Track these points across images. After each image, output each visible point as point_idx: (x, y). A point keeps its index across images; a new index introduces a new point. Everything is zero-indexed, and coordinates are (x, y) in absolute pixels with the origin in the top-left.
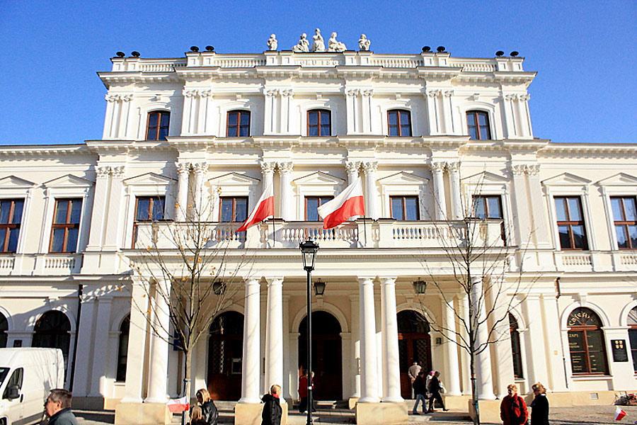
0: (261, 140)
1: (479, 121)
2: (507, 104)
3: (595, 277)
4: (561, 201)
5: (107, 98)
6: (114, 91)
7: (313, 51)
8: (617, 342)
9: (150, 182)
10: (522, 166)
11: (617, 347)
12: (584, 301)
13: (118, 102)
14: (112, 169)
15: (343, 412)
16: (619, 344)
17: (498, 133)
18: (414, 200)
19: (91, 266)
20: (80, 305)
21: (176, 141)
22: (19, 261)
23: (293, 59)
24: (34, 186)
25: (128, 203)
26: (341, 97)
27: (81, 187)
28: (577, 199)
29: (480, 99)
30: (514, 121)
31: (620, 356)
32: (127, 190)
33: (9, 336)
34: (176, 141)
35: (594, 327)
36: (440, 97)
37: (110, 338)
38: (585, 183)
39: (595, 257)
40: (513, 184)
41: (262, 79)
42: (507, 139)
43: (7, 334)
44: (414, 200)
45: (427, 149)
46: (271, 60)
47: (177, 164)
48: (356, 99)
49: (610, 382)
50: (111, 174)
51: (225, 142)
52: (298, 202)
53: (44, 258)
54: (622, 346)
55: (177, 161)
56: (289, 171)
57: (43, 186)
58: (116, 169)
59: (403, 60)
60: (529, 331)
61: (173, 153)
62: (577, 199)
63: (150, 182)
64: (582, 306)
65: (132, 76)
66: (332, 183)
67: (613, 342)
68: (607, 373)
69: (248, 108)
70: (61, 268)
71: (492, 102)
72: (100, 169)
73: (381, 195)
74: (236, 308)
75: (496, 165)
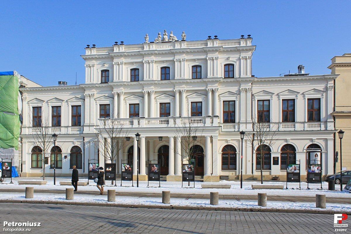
0: (206, 80)
1: (229, 69)
2: (242, 61)
3: (296, 132)
4: (286, 101)
5: (85, 66)
6: (115, 60)
7: (163, 42)
8: (275, 158)
9: (227, 95)
10: (244, 89)
11: (275, 159)
12: (315, 141)
13: (89, 67)
14: (90, 95)
15: (65, 180)
16: (276, 158)
17: (237, 75)
18: (268, 101)
19: (86, 130)
20: (84, 144)
21: (112, 84)
22: (62, 129)
23: (154, 47)
24: (44, 102)
25: (157, 106)
26: (206, 60)
27: (40, 103)
28: (318, 100)
29: (231, 59)
30: (243, 70)
31: (276, 162)
32: (96, 103)
33: (62, 154)
34: (112, 84)
35: (232, 152)
36: (213, 60)
37: (95, 155)
38: (296, 94)
39: (271, 125)
40: (240, 96)
41: (142, 55)
42: (240, 77)
43: (62, 154)
44: (268, 101)
45: (206, 84)
46: (146, 48)
47: (113, 93)
48: (89, 68)
49: (270, 172)
50: (90, 96)
51: (129, 84)
52: (305, 102)
53: (70, 128)
54: (277, 159)
55: (84, 93)
56: (185, 93)
57: (67, 101)
58: (249, 89)
59: (197, 43)
60: (327, 152)
61: (112, 88)
62: (318, 100)
63: (227, 95)
64: (288, 143)
65: (94, 57)
66: (201, 97)
67: (274, 158)
68: (270, 169)
69: (169, 66)
70: (75, 131)
71: (235, 61)
72: (86, 95)
73: (156, 103)
74: (167, 144)
75: (234, 89)
